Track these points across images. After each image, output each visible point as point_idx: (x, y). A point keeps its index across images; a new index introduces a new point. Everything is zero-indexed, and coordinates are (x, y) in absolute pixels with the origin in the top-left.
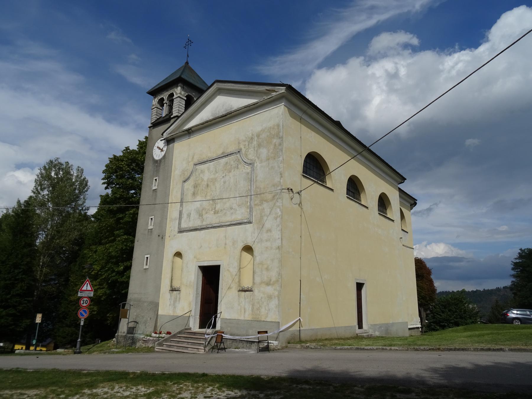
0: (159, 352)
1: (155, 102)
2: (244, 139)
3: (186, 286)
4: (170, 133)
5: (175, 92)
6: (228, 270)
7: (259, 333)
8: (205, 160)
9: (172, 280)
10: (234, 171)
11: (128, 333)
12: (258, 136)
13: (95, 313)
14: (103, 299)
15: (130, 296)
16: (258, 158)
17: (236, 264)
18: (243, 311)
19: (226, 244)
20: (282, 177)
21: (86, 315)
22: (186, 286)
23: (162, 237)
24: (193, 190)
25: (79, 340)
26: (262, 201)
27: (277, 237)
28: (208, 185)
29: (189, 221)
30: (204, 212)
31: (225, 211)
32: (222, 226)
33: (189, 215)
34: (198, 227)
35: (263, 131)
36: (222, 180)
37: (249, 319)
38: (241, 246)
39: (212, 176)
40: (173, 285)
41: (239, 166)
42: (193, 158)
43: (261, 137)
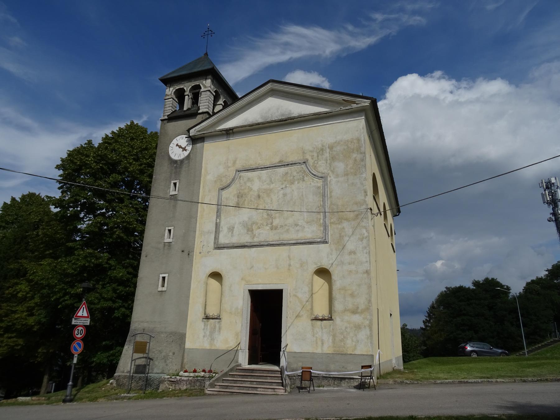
0: (213, 395)
1: (170, 91)
2: (311, 149)
3: (231, 313)
4: (199, 131)
5: (203, 84)
6: (295, 296)
7: (363, 367)
8: (254, 167)
9: (206, 305)
10: (298, 183)
11: (136, 372)
12: (331, 148)
13: (19, 347)
14: (35, 329)
15: (133, 326)
16: (333, 172)
17: (306, 289)
18: (320, 343)
19: (290, 265)
20: (367, 195)
21: (80, 350)
22: (231, 313)
24: (236, 200)
25: (70, 383)
26: (340, 220)
27: (364, 260)
28: (259, 196)
29: (232, 236)
30: (254, 227)
31: (287, 227)
32: (284, 245)
33: (231, 229)
34: (246, 244)
35: (338, 143)
36: (282, 192)
37: (330, 352)
38: (313, 268)
39: (265, 186)
40: (207, 312)
41: (306, 178)
42: (234, 162)
43: (335, 149)
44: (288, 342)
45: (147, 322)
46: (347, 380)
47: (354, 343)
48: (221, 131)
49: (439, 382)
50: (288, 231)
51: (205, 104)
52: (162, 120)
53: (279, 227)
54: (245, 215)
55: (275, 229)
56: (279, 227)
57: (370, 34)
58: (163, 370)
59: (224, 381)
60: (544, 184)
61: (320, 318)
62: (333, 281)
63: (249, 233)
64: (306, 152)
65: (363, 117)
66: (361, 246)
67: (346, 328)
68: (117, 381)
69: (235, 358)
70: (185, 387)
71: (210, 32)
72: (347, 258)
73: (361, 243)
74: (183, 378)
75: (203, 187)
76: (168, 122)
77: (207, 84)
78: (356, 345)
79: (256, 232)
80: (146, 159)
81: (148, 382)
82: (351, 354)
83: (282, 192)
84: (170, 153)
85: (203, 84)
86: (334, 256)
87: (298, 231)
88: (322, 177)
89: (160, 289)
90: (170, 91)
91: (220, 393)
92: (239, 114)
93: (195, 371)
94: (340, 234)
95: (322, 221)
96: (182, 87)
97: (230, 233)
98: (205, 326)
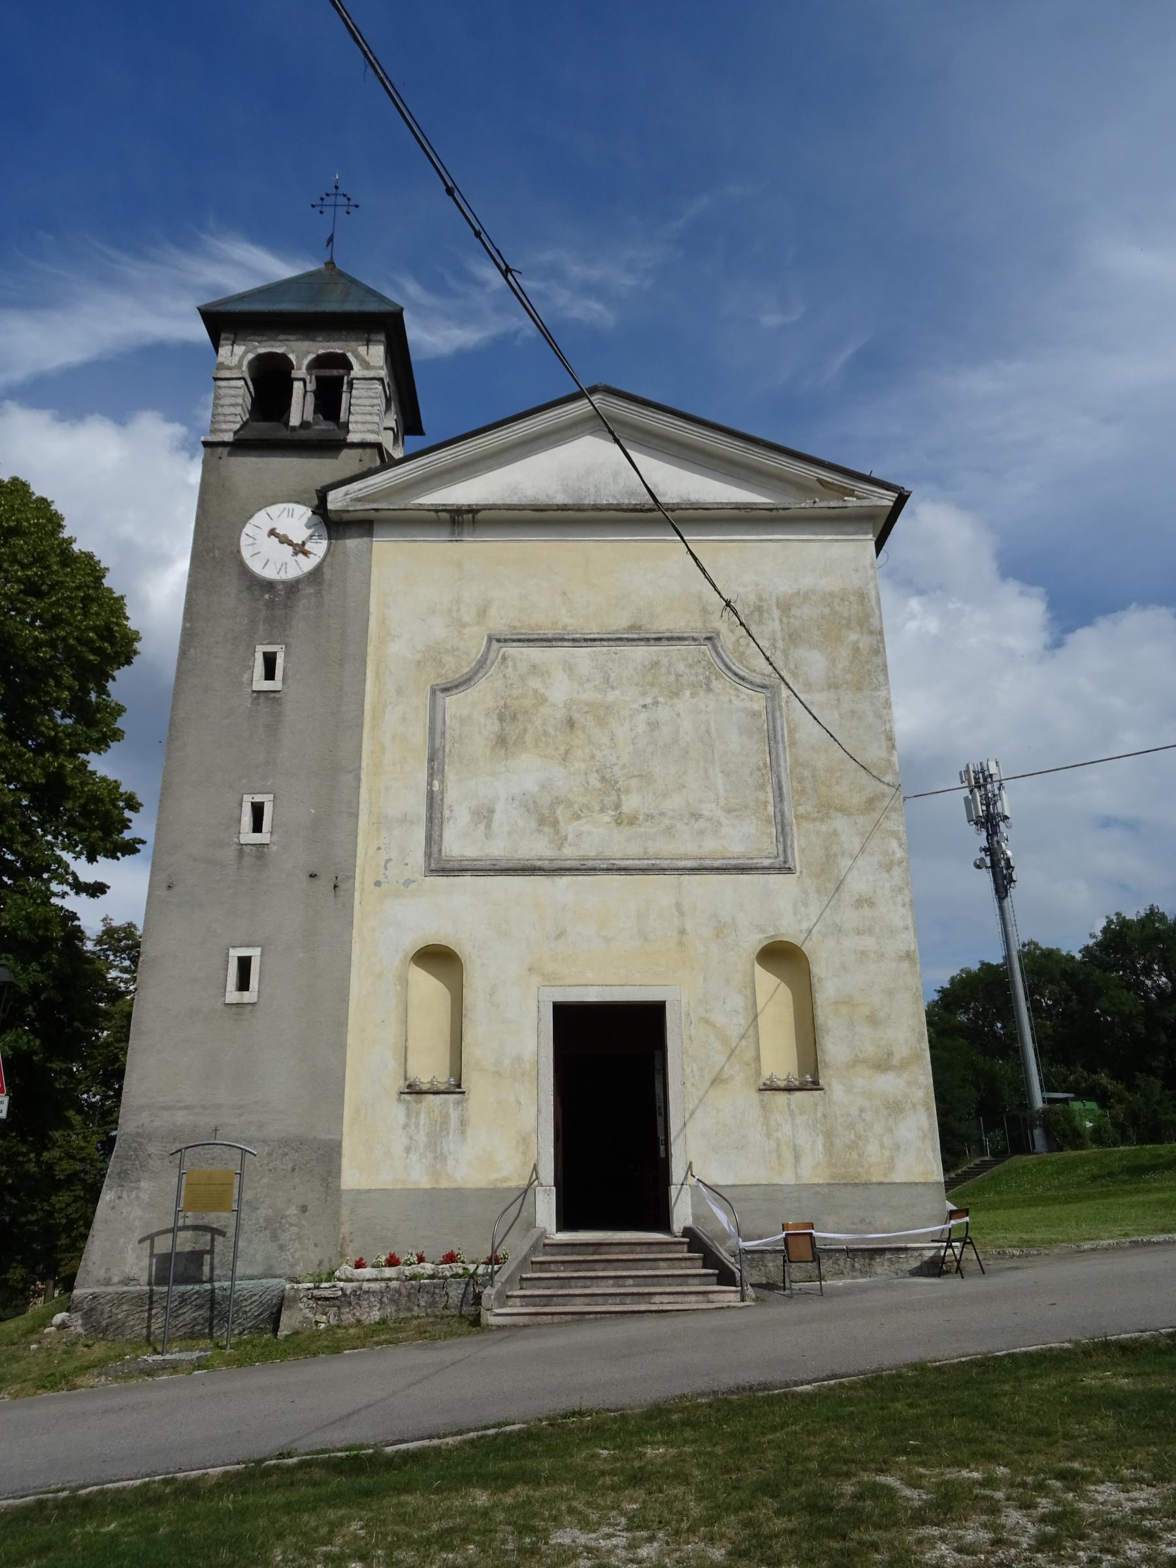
3: (498, 1074)
4: (359, 500)
6: (706, 1021)
10: (693, 695)
11: (161, 1278)
12: (785, 607)
17: (737, 1001)
18: (788, 1155)
19: (682, 932)
22: (498, 1074)
23: (333, 881)
29: (488, 836)
32: (662, 870)
33: (484, 815)
34: (539, 863)
35: (805, 597)
38: (754, 941)
39: (589, 695)
41: (715, 684)
42: (483, 613)
43: (795, 611)
44: (692, 1156)
45: (186, 1108)
46: (888, 1256)
47: (887, 1153)
48: (437, 510)
49: (1086, 1247)
50: (669, 831)
51: (368, 418)
52: (206, 444)
53: (641, 818)
54: (528, 772)
55: (631, 824)
56: (641, 818)
57: (466, 318)
58: (271, 1267)
59: (525, 1284)
60: (972, 775)
61: (782, 1084)
62: (814, 981)
63: (546, 829)
64: (710, 609)
65: (870, 536)
66: (887, 886)
67: (862, 1110)
68: (87, 1315)
69: (524, 1214)
70: (376, 1315)
71: (342, 200)
72: (850, 917)
73: (886, 875)
74: (366, 1286)
75: (378, 676)
76: (230, 455)
77: (369, 358)
78: (892, 1158)
79: (570, 829)
80: (24, 567)
81: (216, 1310)
82: (881, 1184)
83: (643, 716)
84: (246, 553)
85: (357, 356)
86: (814, 911)
87: (701, 832)
88: (764, 687)
89: (233, 996)
90: (237, 355)
91: (539, 1319)
92: (491, 469)
93: (392, 1262)
94: (827, 849)
95: (771, 809)
96: (279, 350)
97: (482, 827)
98: (408, 1116)
